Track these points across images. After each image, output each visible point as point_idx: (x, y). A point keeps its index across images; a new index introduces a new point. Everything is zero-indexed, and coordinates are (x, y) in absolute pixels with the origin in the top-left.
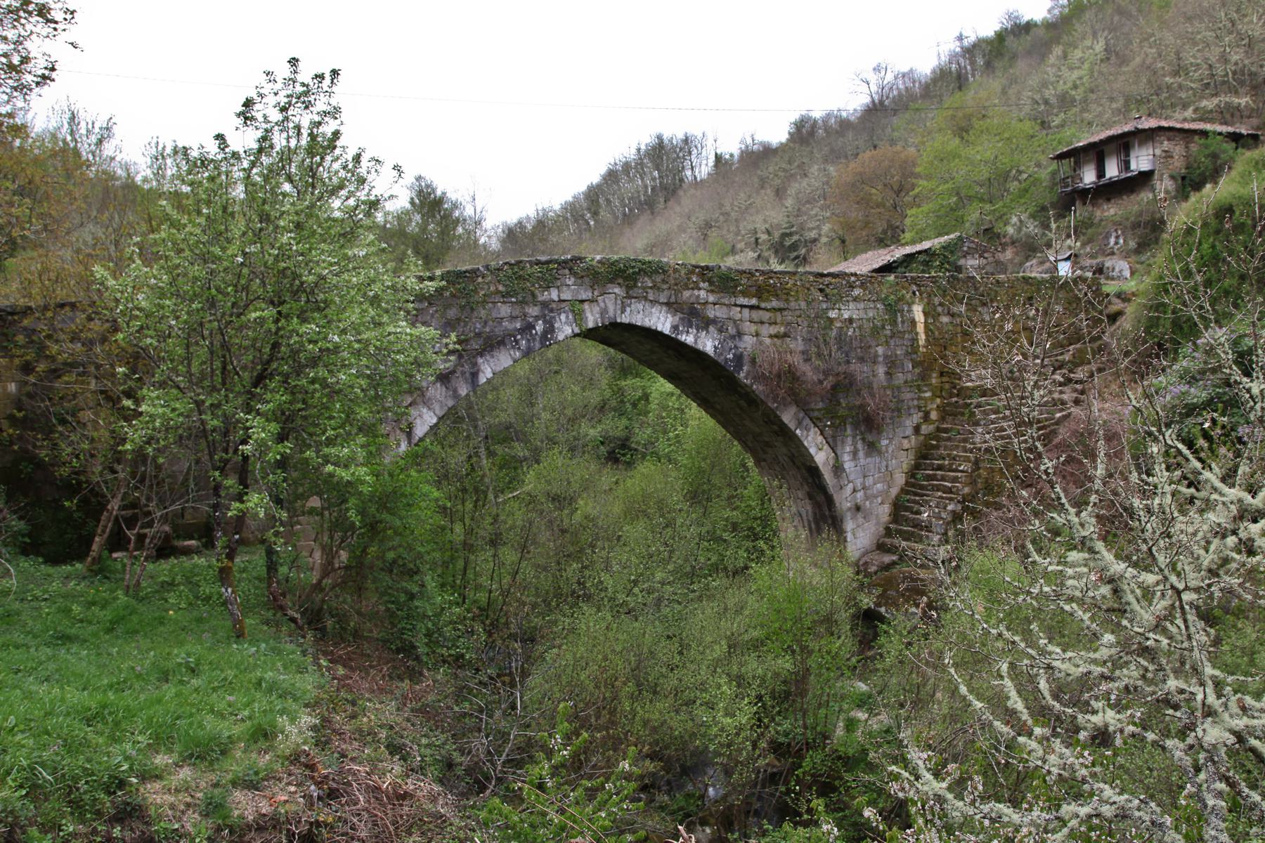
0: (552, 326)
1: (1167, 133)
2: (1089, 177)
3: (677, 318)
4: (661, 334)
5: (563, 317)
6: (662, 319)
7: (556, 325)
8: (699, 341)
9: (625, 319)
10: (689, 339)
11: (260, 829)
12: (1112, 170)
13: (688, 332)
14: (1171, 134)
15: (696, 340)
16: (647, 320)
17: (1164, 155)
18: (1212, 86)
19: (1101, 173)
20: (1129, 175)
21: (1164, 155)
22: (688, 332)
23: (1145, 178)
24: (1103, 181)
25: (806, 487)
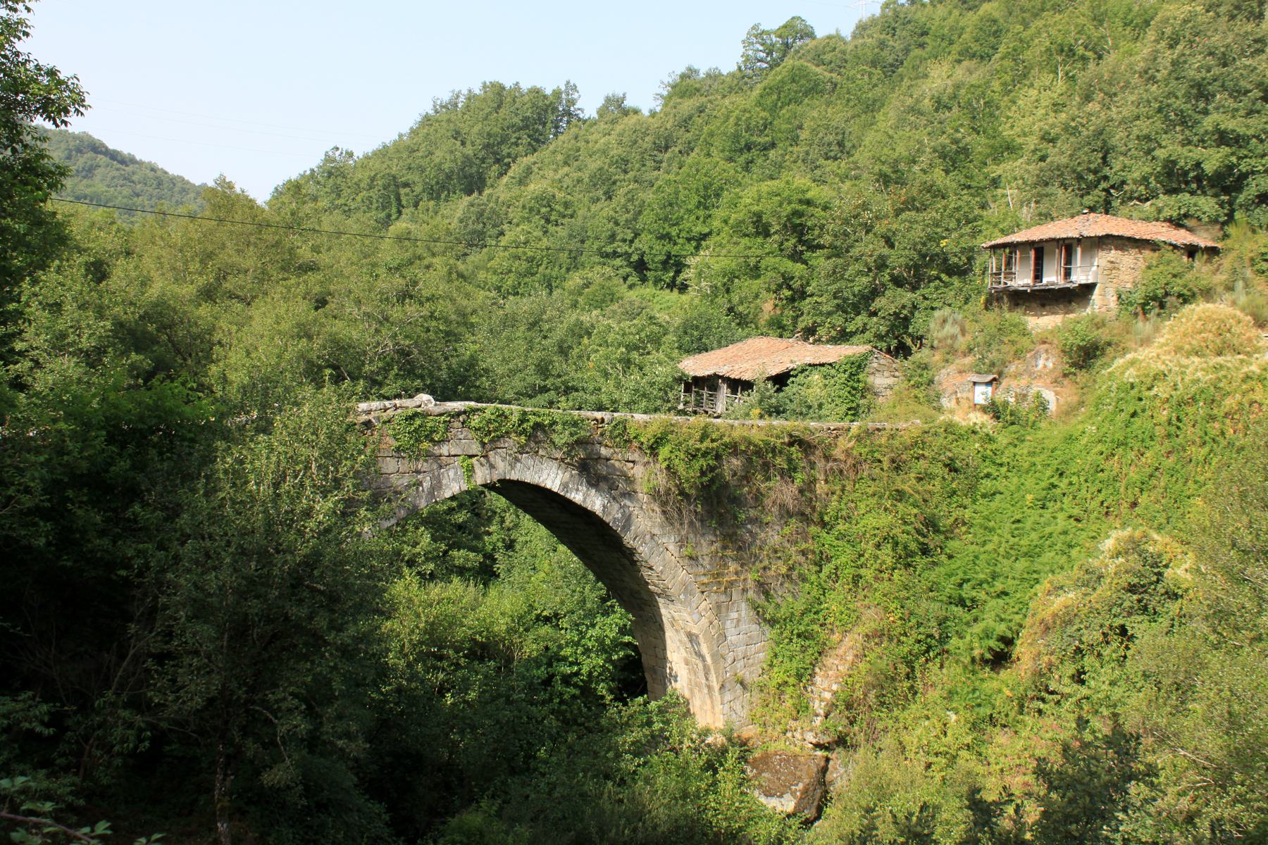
0: (440, 482)
1: (1115, 242)
2: (1023, 280)
3: (567, 475)
4: (550, 491)
5: (451, 473)
6: (553, 475)
7: (444, 482)
8: (588, 500)
9: (514, 476)
10: (577, 497)
11: (6, 403)
12: (1052, 278)
13: (577, 490)
14: (1120, 242)
15: (585, 499)
16: (536, 477)
17: (1110, 265)
18: (1207, 758)
19: (1038, 276)
20: (1068, 285)
21: (1110, 265)
22: (577, 490)
23: (1088, 289)
24: (1039, 286)
25: (682, 650)
